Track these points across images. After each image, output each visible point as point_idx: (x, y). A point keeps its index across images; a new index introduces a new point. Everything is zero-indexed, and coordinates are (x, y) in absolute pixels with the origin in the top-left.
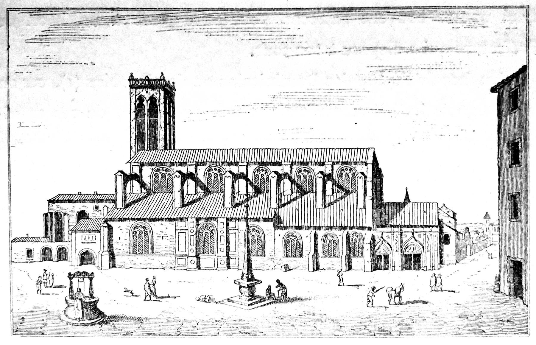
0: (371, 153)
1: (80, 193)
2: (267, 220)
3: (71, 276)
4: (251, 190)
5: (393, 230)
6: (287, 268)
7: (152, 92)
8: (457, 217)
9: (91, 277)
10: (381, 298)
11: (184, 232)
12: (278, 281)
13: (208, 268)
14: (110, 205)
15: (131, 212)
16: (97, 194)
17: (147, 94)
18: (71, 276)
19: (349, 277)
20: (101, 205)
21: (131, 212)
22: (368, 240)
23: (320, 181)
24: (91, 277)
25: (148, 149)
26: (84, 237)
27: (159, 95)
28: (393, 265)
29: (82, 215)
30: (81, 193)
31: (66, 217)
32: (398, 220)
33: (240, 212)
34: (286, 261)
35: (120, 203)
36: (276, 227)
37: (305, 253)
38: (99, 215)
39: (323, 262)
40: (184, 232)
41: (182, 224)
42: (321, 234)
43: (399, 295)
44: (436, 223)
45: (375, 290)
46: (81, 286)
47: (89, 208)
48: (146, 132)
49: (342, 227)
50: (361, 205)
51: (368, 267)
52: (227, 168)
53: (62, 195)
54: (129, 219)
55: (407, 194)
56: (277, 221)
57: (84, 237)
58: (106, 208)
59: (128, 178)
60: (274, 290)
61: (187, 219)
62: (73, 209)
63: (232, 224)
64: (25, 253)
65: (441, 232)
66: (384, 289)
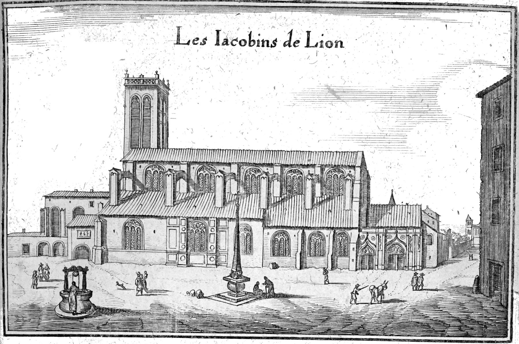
0: (360, 155)
1: (76, 191)
2: (258, 220)
3: (66, 270)
4: (242, 191)
5: (377, 231)
6: (275, 266)
7: (147, 91)
8: (441, 219)
9: (85, 271)
10: (365, 296)
11: (175, 229)
12: (265, 278)
13: (200, 266)
14: (105, 201)
15: (124, 209)
16: (93, 192)
17: (142, 93)
18: (66, 270)
19: (333, 276)
20: (96, 201)
21: (124, 209)
22: (354, 239)
23: (309, 183)
24: (85, 271)
25: (142, 147)
26: (79, 232)
27: (154, 93)
28: (377, 264)
29: (78, 212)
30: (77, 190)
31: (62, 212)
32: (385, 221)
33: (229, 212)
34: (275, 259)
35: (113, 200)
36: (265, 227)
37: (293, 252)
38: (94, 211)
39: (309, 260)
40: (175, 229)
41: (173, 221)
42: (308, 232)
43: (381, 293)
44: (418, 225)
45: (359, 288)
46: (76, 279)
47: (84, 204)
48: (503, 286)
49: (429, 216)
50: (348, 207)
51: (353, 266)
52: (218, 168)
53: (66, 191)
54: (121, 216)
55: (392, 196)
56: (264, 220)
57: (79, 232)
58: (101, 205)
59: (125, 175)
60: (262, 287)
61: (179, 217)
62: (69, 206)
63: (222, 223)
64: (20, 248)
65: (423, 233)
66: (368, 287)
